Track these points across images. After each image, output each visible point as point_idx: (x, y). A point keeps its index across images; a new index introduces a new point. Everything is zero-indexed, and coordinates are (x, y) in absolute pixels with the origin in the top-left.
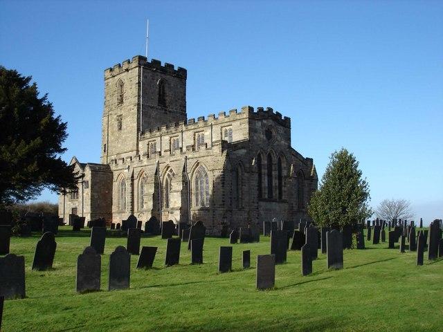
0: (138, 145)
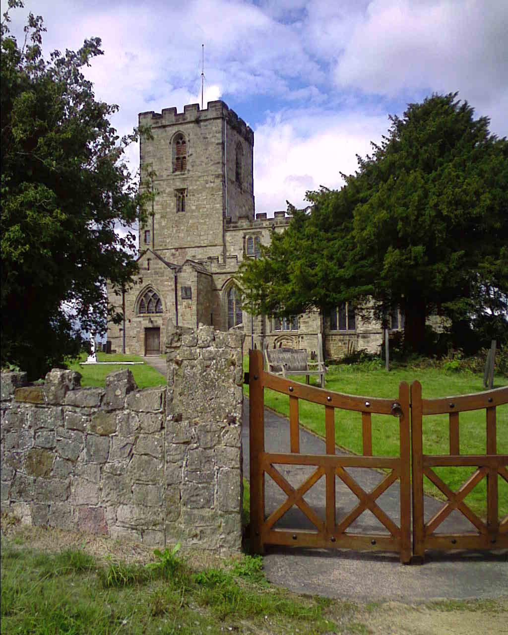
0: (224, 236)
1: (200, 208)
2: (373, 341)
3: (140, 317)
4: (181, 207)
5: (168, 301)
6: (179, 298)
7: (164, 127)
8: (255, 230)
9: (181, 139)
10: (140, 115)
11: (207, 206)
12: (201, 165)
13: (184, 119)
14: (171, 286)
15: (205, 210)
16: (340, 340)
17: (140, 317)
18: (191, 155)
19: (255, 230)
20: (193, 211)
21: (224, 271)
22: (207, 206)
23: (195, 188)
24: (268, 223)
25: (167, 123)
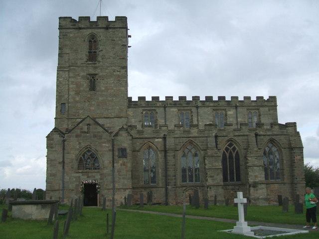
1: (109, 89)
2: (260, 189)
3: (80, 172)
4: (93, 87)
5: (105, 159)
6: (116, 158)
7: (80, 28)
8: (152, 108)
9: (93, 39)
10: (60, 18)
11: (114, 88)
12: (110, 58)
13: (97, 26)
14: (109, 147)
15: (113, 91)
16: (232, 189)
17: (80, 172)
18: (102, 50)
19: (152, 108)
20: (103, 91)
21: (141, 136)
22: (114, 88)
23: (104, 74)
24: (160, 104)
25: (83, 26)
